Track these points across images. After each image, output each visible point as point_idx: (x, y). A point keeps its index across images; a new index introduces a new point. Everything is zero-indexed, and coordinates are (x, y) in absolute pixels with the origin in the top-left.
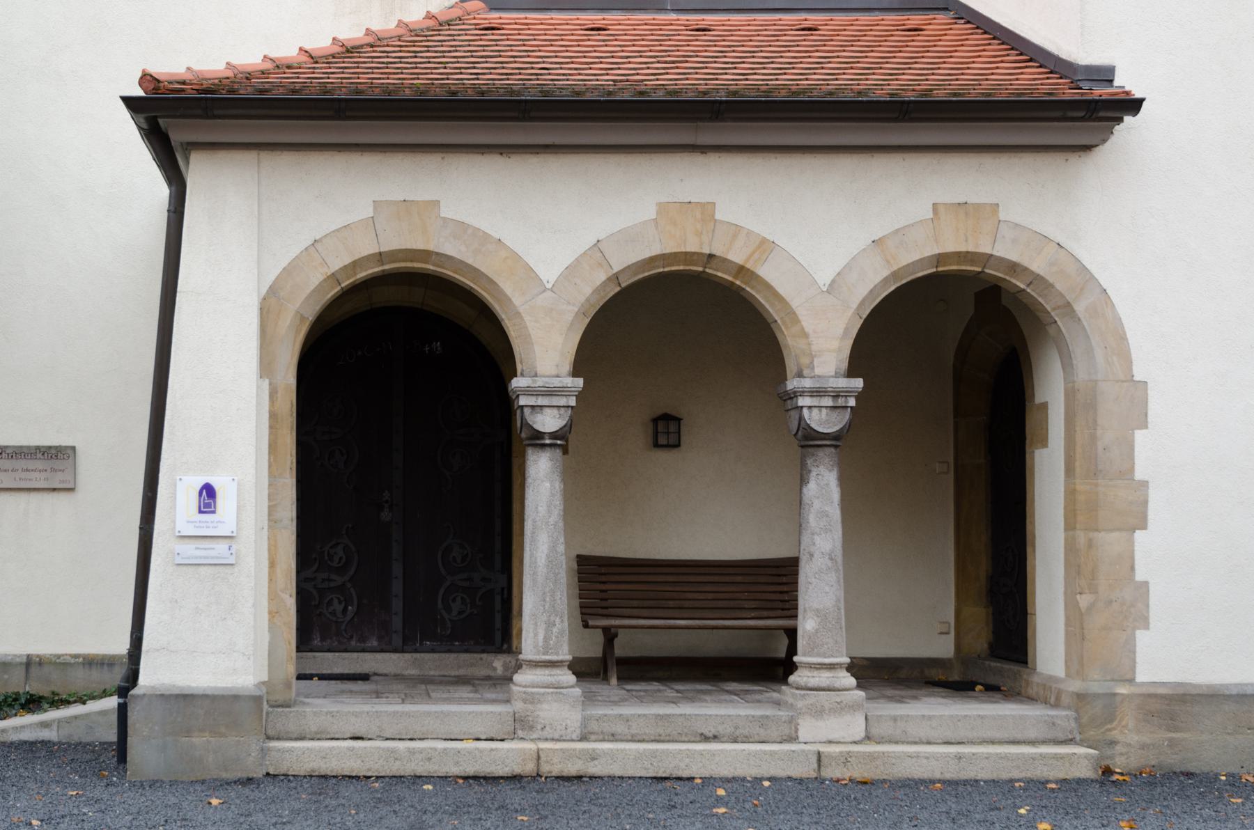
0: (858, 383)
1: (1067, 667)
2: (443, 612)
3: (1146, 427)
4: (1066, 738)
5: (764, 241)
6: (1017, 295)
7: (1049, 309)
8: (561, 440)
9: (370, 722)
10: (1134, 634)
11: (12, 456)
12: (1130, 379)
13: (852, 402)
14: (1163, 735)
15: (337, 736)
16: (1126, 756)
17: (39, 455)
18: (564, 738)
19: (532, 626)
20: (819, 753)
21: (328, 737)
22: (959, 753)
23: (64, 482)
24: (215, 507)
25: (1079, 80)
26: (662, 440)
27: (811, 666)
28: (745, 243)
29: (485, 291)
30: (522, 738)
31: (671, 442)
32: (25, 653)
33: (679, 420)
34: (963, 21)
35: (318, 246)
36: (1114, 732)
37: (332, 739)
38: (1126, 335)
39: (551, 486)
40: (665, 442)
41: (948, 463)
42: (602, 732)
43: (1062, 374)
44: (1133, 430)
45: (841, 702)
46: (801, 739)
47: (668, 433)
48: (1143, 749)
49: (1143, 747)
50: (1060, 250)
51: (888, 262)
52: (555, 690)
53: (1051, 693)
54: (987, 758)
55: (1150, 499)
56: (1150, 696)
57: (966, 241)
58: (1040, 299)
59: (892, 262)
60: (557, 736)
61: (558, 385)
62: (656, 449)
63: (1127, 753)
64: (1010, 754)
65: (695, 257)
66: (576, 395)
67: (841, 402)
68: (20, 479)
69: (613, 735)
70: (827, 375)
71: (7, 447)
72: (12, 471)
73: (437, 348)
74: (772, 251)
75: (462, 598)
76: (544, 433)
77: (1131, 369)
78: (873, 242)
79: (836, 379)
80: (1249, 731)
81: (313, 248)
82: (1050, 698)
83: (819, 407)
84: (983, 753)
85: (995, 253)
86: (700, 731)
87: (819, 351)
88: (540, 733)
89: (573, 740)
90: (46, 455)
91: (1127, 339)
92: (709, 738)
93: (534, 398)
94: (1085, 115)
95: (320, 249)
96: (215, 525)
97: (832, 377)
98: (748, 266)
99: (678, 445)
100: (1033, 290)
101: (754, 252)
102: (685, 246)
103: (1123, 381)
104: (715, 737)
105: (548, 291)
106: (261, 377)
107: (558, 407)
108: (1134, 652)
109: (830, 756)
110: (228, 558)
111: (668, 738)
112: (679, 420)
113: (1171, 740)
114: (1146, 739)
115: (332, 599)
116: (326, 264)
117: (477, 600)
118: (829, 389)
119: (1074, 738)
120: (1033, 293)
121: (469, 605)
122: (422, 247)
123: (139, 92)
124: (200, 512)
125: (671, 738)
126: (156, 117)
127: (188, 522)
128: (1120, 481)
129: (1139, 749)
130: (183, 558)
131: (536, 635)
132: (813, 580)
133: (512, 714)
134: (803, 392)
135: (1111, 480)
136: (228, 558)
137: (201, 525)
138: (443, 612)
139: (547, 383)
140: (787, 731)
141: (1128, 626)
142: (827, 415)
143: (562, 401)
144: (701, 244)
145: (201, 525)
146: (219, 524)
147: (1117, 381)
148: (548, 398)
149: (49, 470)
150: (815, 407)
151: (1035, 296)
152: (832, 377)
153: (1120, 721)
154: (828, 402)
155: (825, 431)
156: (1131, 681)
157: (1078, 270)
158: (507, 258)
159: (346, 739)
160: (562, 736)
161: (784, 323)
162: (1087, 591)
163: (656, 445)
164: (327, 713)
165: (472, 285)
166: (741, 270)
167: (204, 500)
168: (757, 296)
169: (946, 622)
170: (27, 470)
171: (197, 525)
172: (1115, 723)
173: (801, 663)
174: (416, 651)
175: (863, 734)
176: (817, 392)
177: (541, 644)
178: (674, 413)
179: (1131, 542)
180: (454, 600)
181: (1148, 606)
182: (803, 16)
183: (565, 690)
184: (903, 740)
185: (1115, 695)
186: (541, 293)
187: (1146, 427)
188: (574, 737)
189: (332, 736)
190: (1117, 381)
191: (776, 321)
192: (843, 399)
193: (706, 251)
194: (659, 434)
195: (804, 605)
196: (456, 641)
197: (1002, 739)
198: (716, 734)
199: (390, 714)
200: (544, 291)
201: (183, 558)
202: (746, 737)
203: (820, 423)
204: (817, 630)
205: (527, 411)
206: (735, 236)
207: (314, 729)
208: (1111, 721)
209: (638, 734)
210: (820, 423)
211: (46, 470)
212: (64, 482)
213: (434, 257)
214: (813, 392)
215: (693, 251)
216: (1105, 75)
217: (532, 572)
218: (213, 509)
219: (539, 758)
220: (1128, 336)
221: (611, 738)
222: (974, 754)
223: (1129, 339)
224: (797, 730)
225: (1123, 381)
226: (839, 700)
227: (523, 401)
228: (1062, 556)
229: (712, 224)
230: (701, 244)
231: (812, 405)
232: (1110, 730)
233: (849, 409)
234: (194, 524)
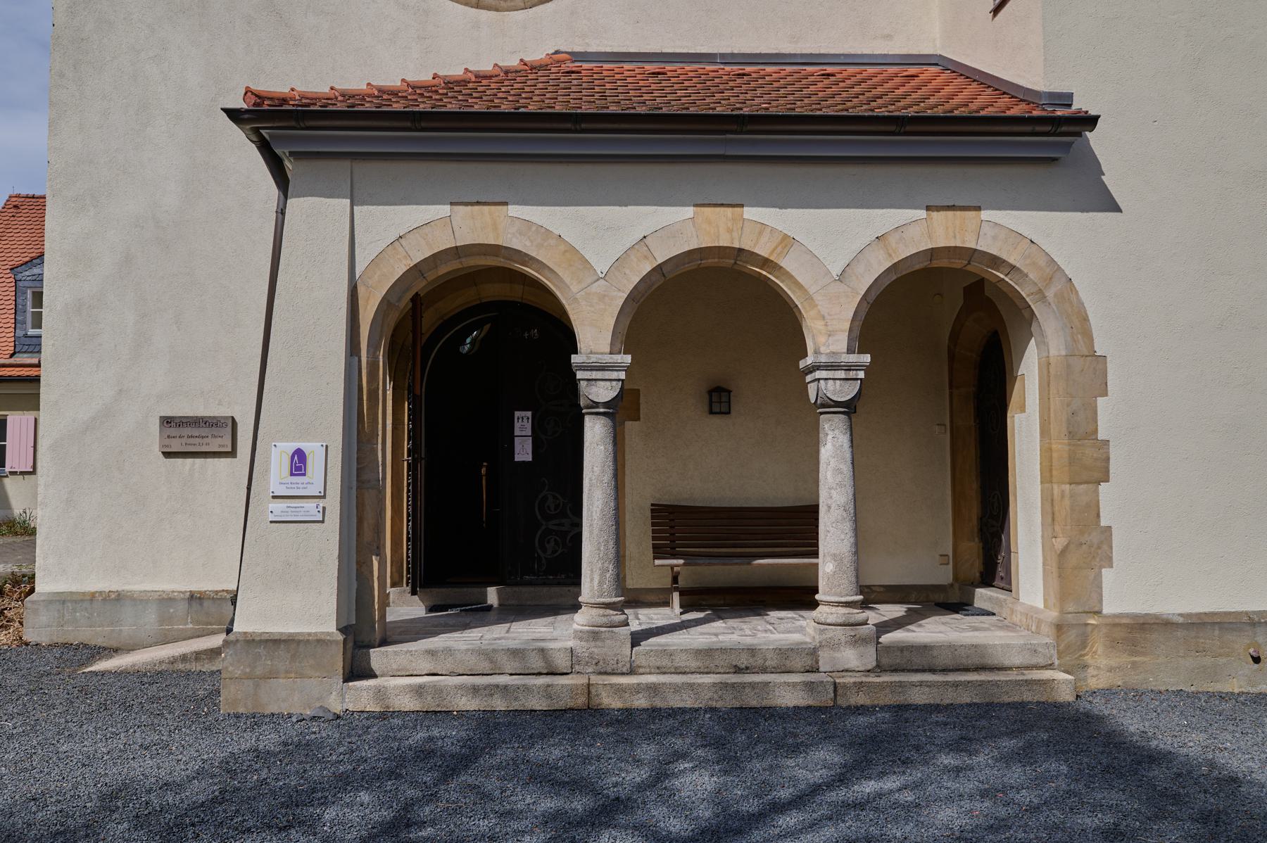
0: (867, 358)
1: (1045, 601)
2: (539, 551)
3: (1106, 395)
4: (1046, 663)
5: (786, 237)
6: (998, 284)
7: (1024, 296)
8: (849, 408)
9: (445, 659)
10: (1101, 572)
11: (179, 425)
12: (1093, 354)
13: (861, 375)
14: (1125, 659)
15: (415, 673)
16: (1096, 679)
17: (202, 424)
18: (616, 671)
19: (589, 572)
20: (835, 683)
21: (407, 674)
22: (956, 681)
23: (223, 446)
24: (305, 470)
25: (1044, 104)
26: (716, 408)
27: (829, 603)
28: (769, 239)
29: (549, 281)
30: (578, 672)
31: (723, 410)
32: (188, 590)
33: (729, 392)
34: (949, 72)
35: (402, 241)
36: (1086, 657)
37: (412, 675)
38: (1088, 317)
39: (605, 449)
40: (718, 411)
41: (945, 425)
42: (649, 666)
43: (1036, 351)
44: (1096, 398)
45: (855, 635)
46: (821, 669)
47: (720, 402)
48: (1111, 671)
49: (1110, 670)
50: (1033, 245)
51: (890, 255)
52: (608, 629)
53: (1033, 621)
54: (980, 685)
55: (1111, 456)
56: (1115, 625)
57: (955, 237)
58: (1016, 287)
59: (893, 255)
60: (609, 670)
61: (610, 361)
62: (711, 416)
63: (1097, 675)
64: (1000, 681)
65: (728, 251)
66: (625, 370)
67: (852, 374)
68: (186, 444)
69: (658, 668)
70: (839, 351)
71: (176, 417)
72: (180, 437)
73: (534, 334)
74: (792, 246)
75: (555, 540)
76: (599, 403)
77: (1093, 346)
78: (877, 238)
79: (848, 355)
80: (1197, 654)
81: (398, 243)
82: (1032, 626)
83: (833, 379)
84: (977, 681)
85: (979, 248)
86: (734, 663)
87: (833, 331)
88: (595, 667)
89: (623, 674)
90: (208, 424)
91: (1089, 320)
92: (742, 669)
93: (589, 373)
94: (1051, 130)
95: (404, 244)
96: (305, 486)
97: (844, 353)
98: (772, 258)
99: (729, 413)
100: (1010, 279)
101: (776, 247)
102: (718, 241)
103: (1087, 356)
104: (747, 668)
105: (601, 280)
106: (351, 355)
107: (610, 380)
108: (1101, 588)
109: (845, 686)
110: (315, 515)
111: (706, 670)
112: (729, 392)
113: (1134, 663)
114: (1113, 663)
115: (555, 510)
116: (409, 256)
117: (567, 541)
118: (842, 364)
119: (1053, 663)
120: (1010, 282)
121: (561, 545)
122: (493, 242)
123: (240, 104)
124: (292, 474)
125: (709, 670)
126: (258, 129)
127: (281, 483)
128: (1086, 441)
129: (1108, 671)
130: (275, 516)
131: (592, 580)
132: (831, 528)
133: (569, 650)
134: (820, 366)
135: (1079, 440)
136: (315, 515)
137: (293, 486)
138: (539, 551)
139: (601, 359)
140: (809, 662)
141: (1095, 565)
142: (840, 386)
143: (614, 375)
144: (732, 239)
145: (293, 486)
146: (309, 486)
147: (1082, 356)
148: (601, 372)
149: (210, 436)
150: (830, 379)
151: (1013, 284)
152: (844, 353)
153: (1092, 646)
154: (841, 374)
155: (839, 400)
156: (1099, 613)
157: (1047, 263)
158: (566, 251)
159: (423, 675)
160: (613, 670)
161: (804, 308)
162: (1061, 536)
163: (711, 412)
164: (406, 653)
165: (536, 274)
166: (766, 263)
167: (296, 463)
168: (781, 284)
169: (947, 555)
170: (192, 437)
171: (290, 486)
172: (1087, 649)
173: (821, 601)
174: (517, 584)
175: (874, 664)
176: (832, 366)
177: (596, 588)
178: (724, 386)
179: (1096, 492)
180: (548, 542)
181: (1111, 547)
182: (824, 67)
183: (617, 629)
184: (908, 668)
185: (1087, 624)
186: (595, 282)
187: (1106, 395)
188: (624, 670)
189: (411, 673)
190: (1082, 356)
191: (797, 306)
192: (854, 372)
193: (736, 245)
194: (713, 404)
195: (824, 550)
196: (550, 575)
197: (993, 665)
198: (748, 665)
199: (462, 652)
200: (598, 280)
201: (275, 516)
202: (774, 668)
203: (834, 392)
204: (835, 572)
205: (583, 384)
206: (760, 233)
207: (395, 667)
208: (1085, 647)
209: (680, 667)
210: (834, 392)
211: (207, 437)
212: (223, 446)
213: (503, 251)
214: (828, 366)
215: (725, 245)
216: (1065, 99)
217: (588, 525)
218: (303, 472)
219: (589, 692)
220: (1090, 318)
221: (657, 671)
222: (969, 682)
223: (1091, 321)
224: (817, 662)
225: (1087, 356)
226: (853, 634)
227: (580, 375)
228: (1039, 504)
229: (741, 222)
230: (732, 239)
231: (828, 377)
232: (1084, 655)
233: (859, 382)
234: (286, 485)
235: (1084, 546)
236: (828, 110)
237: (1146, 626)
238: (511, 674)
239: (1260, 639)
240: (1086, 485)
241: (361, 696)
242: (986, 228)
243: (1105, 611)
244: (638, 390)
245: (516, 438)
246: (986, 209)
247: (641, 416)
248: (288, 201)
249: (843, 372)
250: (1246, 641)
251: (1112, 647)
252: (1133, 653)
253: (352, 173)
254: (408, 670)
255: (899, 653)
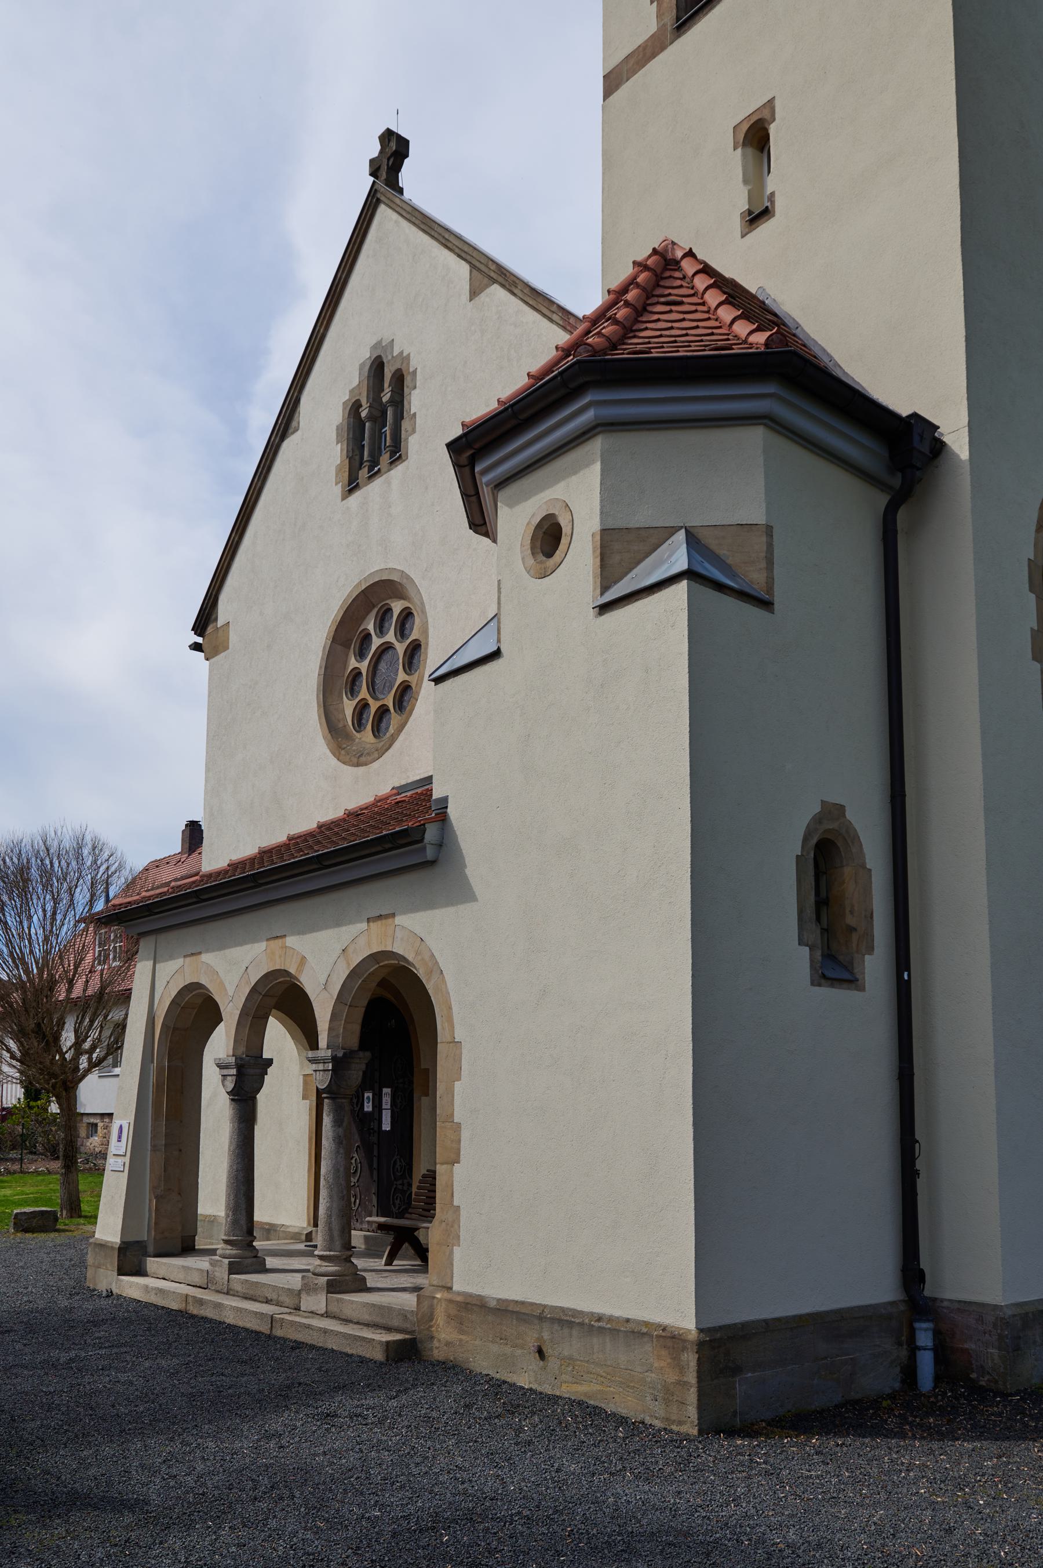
179: (452, 1171)
185: (435, 1297)
235: (444, 1223)
236: (35, 918)
237: (469, 1306)
238: (188, 1285)
239: (546, 1335)
240: (446, 1165)
241: (132, 1287)
242: (399, 934)
243: (455, 1288)
244: (428, 1069)
245: (384, 1111)
246: (289, 936)
247: (430, 1092)
248: (157, 966)
249: (322, 1064)
250: (535, 1335)
251: (448, 1322)
252: (461, 1332)
253: (156, 947)
254: (156, 1274)
255: (336, 1303)
